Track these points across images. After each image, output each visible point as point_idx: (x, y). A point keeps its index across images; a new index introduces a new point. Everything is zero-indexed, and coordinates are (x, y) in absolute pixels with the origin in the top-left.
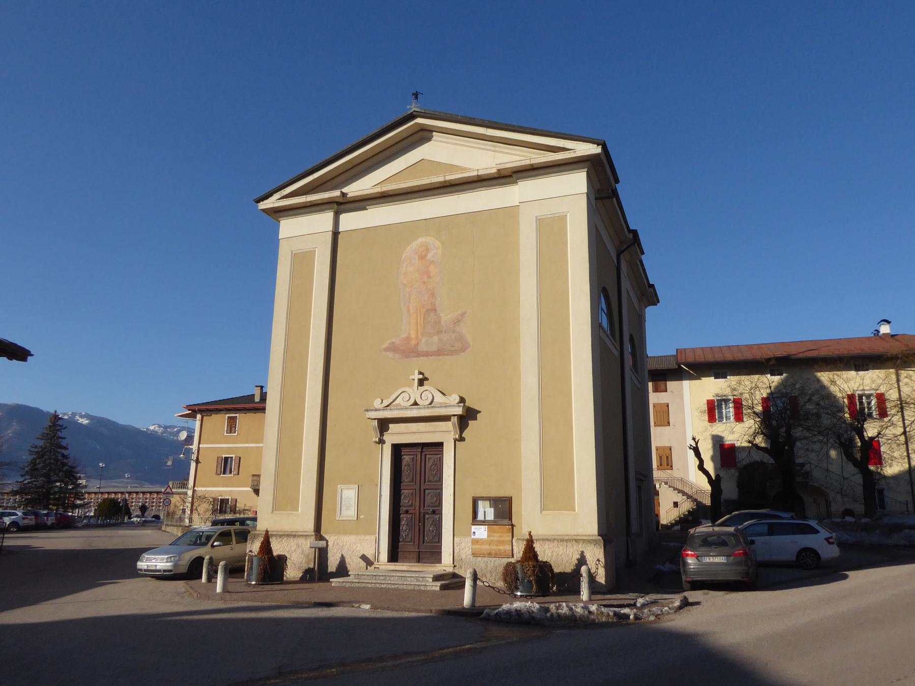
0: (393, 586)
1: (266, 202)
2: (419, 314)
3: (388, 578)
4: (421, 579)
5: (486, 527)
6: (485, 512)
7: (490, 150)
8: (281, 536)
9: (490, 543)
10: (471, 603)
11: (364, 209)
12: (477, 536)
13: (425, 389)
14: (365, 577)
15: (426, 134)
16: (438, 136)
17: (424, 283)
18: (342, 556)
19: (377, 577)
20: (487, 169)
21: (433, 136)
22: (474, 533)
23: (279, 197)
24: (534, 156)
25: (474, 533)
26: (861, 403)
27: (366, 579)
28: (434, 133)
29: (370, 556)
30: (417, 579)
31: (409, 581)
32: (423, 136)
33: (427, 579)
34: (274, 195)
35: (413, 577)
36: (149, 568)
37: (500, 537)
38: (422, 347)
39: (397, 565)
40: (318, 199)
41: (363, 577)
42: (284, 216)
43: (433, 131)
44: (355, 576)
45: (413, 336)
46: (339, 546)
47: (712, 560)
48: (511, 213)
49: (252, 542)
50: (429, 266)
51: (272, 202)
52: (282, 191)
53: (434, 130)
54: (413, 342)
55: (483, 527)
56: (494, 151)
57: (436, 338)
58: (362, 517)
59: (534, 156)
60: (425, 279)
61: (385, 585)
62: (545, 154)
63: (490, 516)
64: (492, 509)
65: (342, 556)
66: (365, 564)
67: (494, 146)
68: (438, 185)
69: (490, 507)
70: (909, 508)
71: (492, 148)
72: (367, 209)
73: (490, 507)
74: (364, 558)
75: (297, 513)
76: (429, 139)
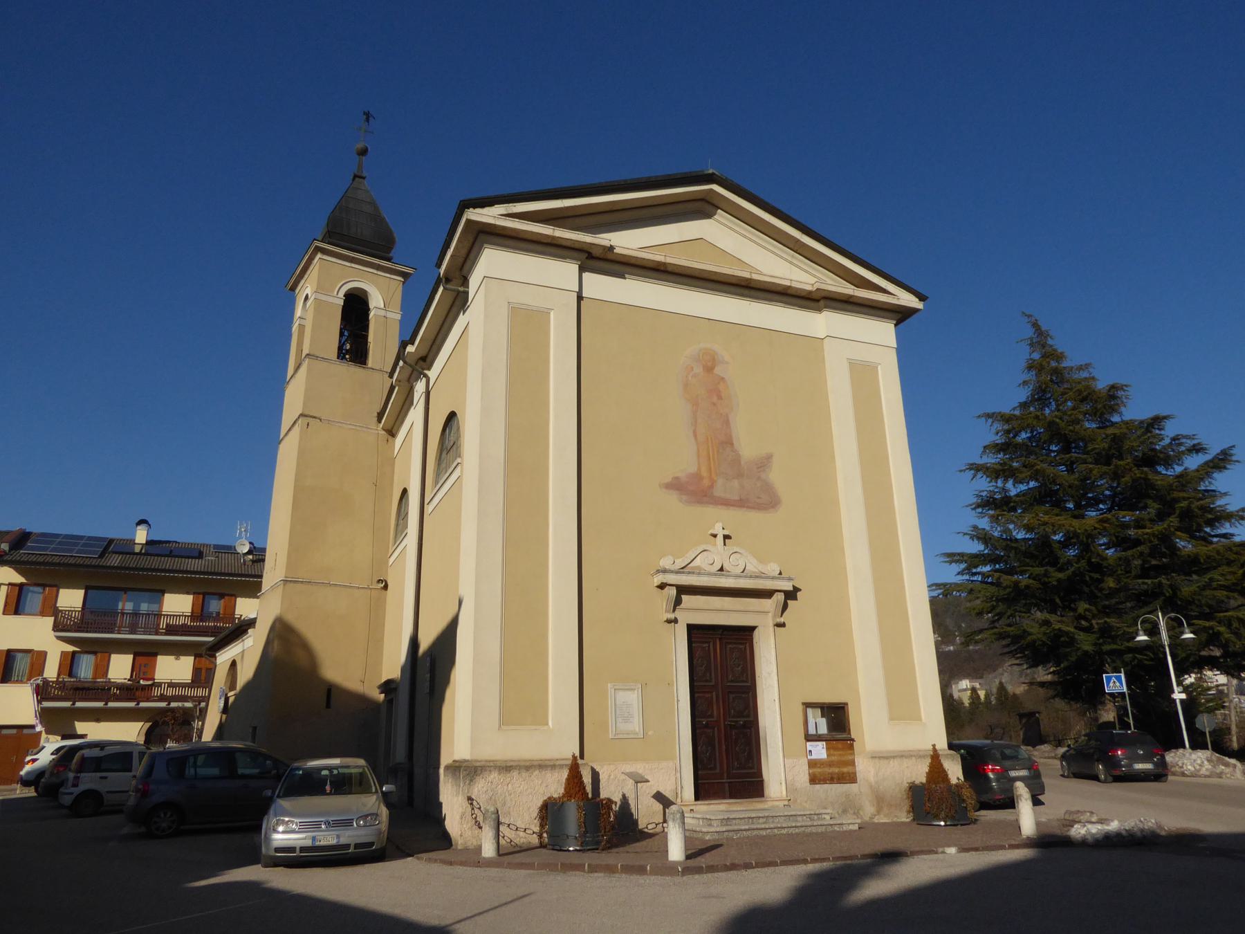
0: (797, 831)
1: (478, 210)
2: (710, 444)
3: (771, 820)
4: (816, 817)
5: (824, 743)
6: (816, 723)
7: (786, 260)
8: (528, 768)
9: (830, 764)
10: (1035, 830)
11: (621, 276)
12: (814, 756)
13: (735, 551)
14: (737, 821)
15: (709, 208)
16: (722, 216)
17: (714, 404)
18: (624, 796)
19: (755, 820)
20: (801, 282)
21: (715, 214)
22: (810, 751)
23: (505, 213)
24: (830, 282)
25: (810, 751)
26: (61, 619)
27: (739, 824)
28: (719, 211)
29: (668, 794)
30: (810, 818)
31: (799, 822)
32: (703, 208)
33: (824, 816)
34: (496, 206)
35: (805, 815)
36: (317, 844)
37: (840, 755)
38: (719, 491)
39: (711, 804)
40: (573, 238)
41: (734, 821)
42: (494, 244)
43: (719, 208)
44: (722, 822)
45: (705, 473)
46: (618, 780)
47: (1017, 774)
48: (814, 344)
49: (471, 781)
50: (719, 383)
51: (490, 215)
52: (511, 205)
53: (720, 206)
54: (706, 482)
55: (820, 744)
56: (791, 263)
57: (736, 483)
58: (650, 733)
59: (830, 282)
60: (715, 399)
61: (786, 830)
62: (841, 283)
63: (823, 729)
64: (824, 720)
65: (624, 796)
66: (661, 806)
67: (793, 256)
68: (734, 281)
69: (822, 717)
70: (809, 729)
71: (789, 259)
72: (625, 278)
73: (822, 717)
74: (659, 797)
75: (546, 727)
76: (709, 216)
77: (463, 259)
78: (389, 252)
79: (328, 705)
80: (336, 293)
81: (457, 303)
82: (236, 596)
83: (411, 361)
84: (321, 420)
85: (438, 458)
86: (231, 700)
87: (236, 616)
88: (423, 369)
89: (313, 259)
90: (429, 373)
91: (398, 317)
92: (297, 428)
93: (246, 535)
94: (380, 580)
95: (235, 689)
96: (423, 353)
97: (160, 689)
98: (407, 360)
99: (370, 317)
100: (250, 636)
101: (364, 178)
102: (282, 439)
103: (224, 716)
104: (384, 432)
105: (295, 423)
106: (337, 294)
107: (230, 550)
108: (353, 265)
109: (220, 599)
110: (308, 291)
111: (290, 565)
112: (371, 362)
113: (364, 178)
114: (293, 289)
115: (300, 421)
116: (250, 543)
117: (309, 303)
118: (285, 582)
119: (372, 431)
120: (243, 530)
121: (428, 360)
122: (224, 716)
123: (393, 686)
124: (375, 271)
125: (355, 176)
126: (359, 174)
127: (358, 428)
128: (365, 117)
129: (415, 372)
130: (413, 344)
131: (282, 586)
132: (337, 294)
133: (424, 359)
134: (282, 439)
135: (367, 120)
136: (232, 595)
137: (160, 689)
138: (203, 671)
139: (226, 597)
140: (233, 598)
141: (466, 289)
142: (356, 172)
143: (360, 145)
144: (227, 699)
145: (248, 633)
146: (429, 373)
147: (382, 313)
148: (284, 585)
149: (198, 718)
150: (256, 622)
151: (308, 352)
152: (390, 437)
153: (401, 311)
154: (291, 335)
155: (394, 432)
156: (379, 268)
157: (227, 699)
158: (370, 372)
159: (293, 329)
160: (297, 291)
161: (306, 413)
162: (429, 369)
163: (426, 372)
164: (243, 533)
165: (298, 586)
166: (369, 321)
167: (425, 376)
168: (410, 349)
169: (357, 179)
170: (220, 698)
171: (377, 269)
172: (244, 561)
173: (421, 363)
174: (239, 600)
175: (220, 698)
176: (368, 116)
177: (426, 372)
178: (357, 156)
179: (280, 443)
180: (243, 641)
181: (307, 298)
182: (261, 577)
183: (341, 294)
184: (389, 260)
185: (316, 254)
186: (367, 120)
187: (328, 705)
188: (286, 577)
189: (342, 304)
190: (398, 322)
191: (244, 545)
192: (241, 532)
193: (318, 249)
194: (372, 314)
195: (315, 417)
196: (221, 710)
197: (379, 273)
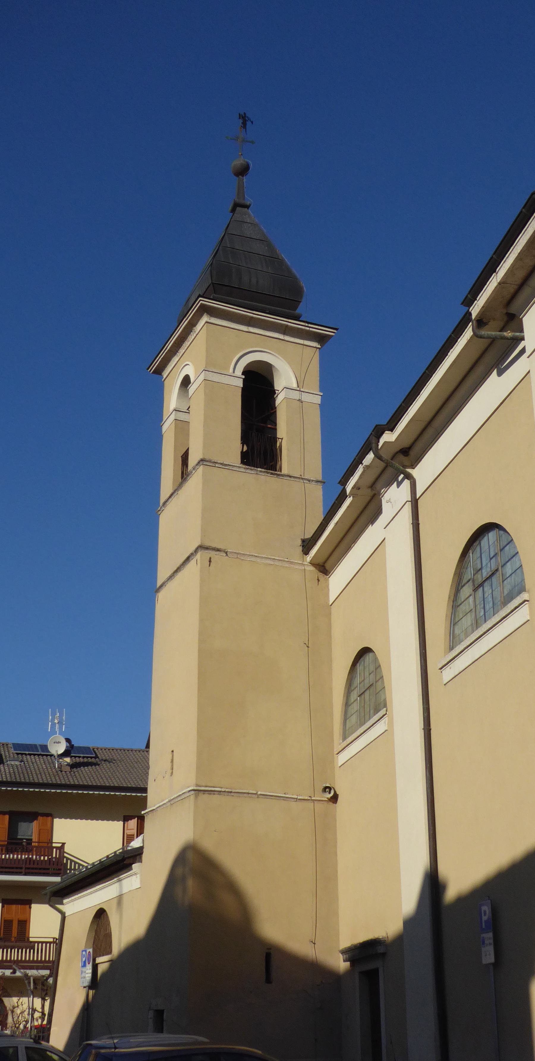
77: (516, 287)
78: (295, 308)
79: (268, 980)
80: (231, 370)
81: (488, 358)
82: (51, 816)
83: (386, 455)
84: (226, 553)
85: (452, 598)
86: (101, 969)
87: (54, 845)
88: (405, 467)
89: (195, 325)
90: (414, 472)
91: (317, 400)
92: (193, 568)
93: (60, 728)
94: (326, 788)
95: (110, 952)
96: (406, 443)
97: (32, 951)
98: (382, 453)
99: (278, 401)
100: (136, 874)
101: (248, 207)
102: (161, 586)
103: (91, 992)
104: (312, 568)
105: (188, 559)
106: (234, 372)
107: (43, 751)
108: (252, 329)
109: (32, 821)
110: (190, 371)
111: (201, 768)
112: (286, 465)
113: (248, 207)
114: (159, 371)
115: (198, 556)
116: (68, 740)
117: (192, 389)
118: (197, 792)
119: (297, 567)
120: (56, 721)
121: (413, 453)
122: (91, 992)
123: (381, 950)
124: (281, 336)
125: (236, 205)
126: (241, 201)
127: (277, 563)
128: (241, 121)
129: (390, 471)
130: (392, 430)
131: (192, 797)
132: (234, 372)
133: (405, 451)
134: (161, 586)
135: (244, 125)
136: (48, 815)
137: (32, 951)
138: (5, 924)
139: (40, 818)
140: (49, 818)
141: (523, 334)
142: (237, 201)
143: (238, 162)
144: (95, 968)
145: (131, 869)
146: (414, 472)
147: (296, 395)
148: (196, 797)
149: (32, 992)
150: (142, 853)
151: (201, 457)
152: (321, 576)
153: (320, 391)
154: (159, 437)
155: (328, 566)
156: (286, 330)
157: (95, 968)
158: (285, 481)
159: (164, 428)
160: (165, 374)
161: (207, 544)
162: (413, 466)
163: (409, 470)
164: (57, 726)
165: (216, 797)
166: (276, 408)
167: (408, 476)
168: (388, 437)
169: (238, 209)
170: (84, 965)
171: (284, 333)
172: (60, 766)
173: (401, 457)
174: (57, 821)
175: (84, 965)
176: (244, 119)
177: (409, 470)
178: (235, 177)
179: (158, 590)
180: (120, 881)
181: (186, 382)
182: (145, 790)
183: (239, 371)
184: (297, 318)
185: (201, 316)
186: (244, 125)
187: (268, 980)
188: (197, 785)
189: (242, 386)
190: (318, 407)
191: (59, 742)
192: (53, 725)
193: (204, 310)
194: (279, 399)
195: (218, 550)
196: (86, 984)
197: (287, 338)
